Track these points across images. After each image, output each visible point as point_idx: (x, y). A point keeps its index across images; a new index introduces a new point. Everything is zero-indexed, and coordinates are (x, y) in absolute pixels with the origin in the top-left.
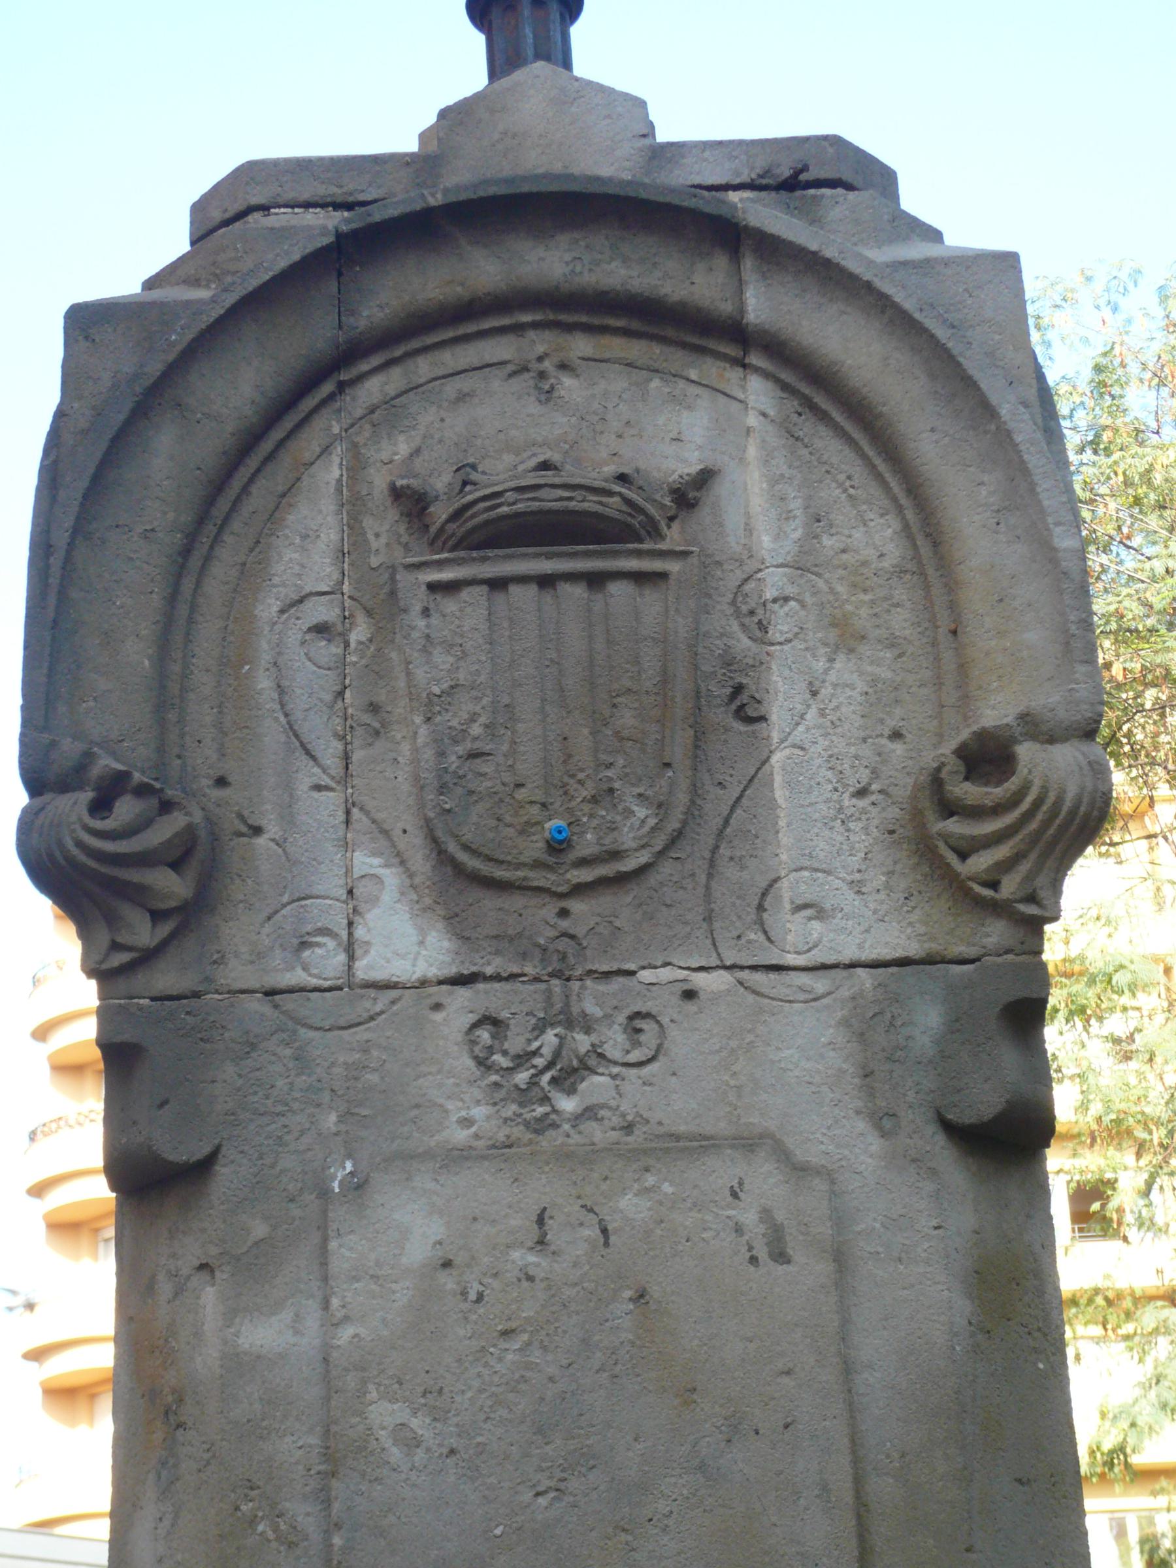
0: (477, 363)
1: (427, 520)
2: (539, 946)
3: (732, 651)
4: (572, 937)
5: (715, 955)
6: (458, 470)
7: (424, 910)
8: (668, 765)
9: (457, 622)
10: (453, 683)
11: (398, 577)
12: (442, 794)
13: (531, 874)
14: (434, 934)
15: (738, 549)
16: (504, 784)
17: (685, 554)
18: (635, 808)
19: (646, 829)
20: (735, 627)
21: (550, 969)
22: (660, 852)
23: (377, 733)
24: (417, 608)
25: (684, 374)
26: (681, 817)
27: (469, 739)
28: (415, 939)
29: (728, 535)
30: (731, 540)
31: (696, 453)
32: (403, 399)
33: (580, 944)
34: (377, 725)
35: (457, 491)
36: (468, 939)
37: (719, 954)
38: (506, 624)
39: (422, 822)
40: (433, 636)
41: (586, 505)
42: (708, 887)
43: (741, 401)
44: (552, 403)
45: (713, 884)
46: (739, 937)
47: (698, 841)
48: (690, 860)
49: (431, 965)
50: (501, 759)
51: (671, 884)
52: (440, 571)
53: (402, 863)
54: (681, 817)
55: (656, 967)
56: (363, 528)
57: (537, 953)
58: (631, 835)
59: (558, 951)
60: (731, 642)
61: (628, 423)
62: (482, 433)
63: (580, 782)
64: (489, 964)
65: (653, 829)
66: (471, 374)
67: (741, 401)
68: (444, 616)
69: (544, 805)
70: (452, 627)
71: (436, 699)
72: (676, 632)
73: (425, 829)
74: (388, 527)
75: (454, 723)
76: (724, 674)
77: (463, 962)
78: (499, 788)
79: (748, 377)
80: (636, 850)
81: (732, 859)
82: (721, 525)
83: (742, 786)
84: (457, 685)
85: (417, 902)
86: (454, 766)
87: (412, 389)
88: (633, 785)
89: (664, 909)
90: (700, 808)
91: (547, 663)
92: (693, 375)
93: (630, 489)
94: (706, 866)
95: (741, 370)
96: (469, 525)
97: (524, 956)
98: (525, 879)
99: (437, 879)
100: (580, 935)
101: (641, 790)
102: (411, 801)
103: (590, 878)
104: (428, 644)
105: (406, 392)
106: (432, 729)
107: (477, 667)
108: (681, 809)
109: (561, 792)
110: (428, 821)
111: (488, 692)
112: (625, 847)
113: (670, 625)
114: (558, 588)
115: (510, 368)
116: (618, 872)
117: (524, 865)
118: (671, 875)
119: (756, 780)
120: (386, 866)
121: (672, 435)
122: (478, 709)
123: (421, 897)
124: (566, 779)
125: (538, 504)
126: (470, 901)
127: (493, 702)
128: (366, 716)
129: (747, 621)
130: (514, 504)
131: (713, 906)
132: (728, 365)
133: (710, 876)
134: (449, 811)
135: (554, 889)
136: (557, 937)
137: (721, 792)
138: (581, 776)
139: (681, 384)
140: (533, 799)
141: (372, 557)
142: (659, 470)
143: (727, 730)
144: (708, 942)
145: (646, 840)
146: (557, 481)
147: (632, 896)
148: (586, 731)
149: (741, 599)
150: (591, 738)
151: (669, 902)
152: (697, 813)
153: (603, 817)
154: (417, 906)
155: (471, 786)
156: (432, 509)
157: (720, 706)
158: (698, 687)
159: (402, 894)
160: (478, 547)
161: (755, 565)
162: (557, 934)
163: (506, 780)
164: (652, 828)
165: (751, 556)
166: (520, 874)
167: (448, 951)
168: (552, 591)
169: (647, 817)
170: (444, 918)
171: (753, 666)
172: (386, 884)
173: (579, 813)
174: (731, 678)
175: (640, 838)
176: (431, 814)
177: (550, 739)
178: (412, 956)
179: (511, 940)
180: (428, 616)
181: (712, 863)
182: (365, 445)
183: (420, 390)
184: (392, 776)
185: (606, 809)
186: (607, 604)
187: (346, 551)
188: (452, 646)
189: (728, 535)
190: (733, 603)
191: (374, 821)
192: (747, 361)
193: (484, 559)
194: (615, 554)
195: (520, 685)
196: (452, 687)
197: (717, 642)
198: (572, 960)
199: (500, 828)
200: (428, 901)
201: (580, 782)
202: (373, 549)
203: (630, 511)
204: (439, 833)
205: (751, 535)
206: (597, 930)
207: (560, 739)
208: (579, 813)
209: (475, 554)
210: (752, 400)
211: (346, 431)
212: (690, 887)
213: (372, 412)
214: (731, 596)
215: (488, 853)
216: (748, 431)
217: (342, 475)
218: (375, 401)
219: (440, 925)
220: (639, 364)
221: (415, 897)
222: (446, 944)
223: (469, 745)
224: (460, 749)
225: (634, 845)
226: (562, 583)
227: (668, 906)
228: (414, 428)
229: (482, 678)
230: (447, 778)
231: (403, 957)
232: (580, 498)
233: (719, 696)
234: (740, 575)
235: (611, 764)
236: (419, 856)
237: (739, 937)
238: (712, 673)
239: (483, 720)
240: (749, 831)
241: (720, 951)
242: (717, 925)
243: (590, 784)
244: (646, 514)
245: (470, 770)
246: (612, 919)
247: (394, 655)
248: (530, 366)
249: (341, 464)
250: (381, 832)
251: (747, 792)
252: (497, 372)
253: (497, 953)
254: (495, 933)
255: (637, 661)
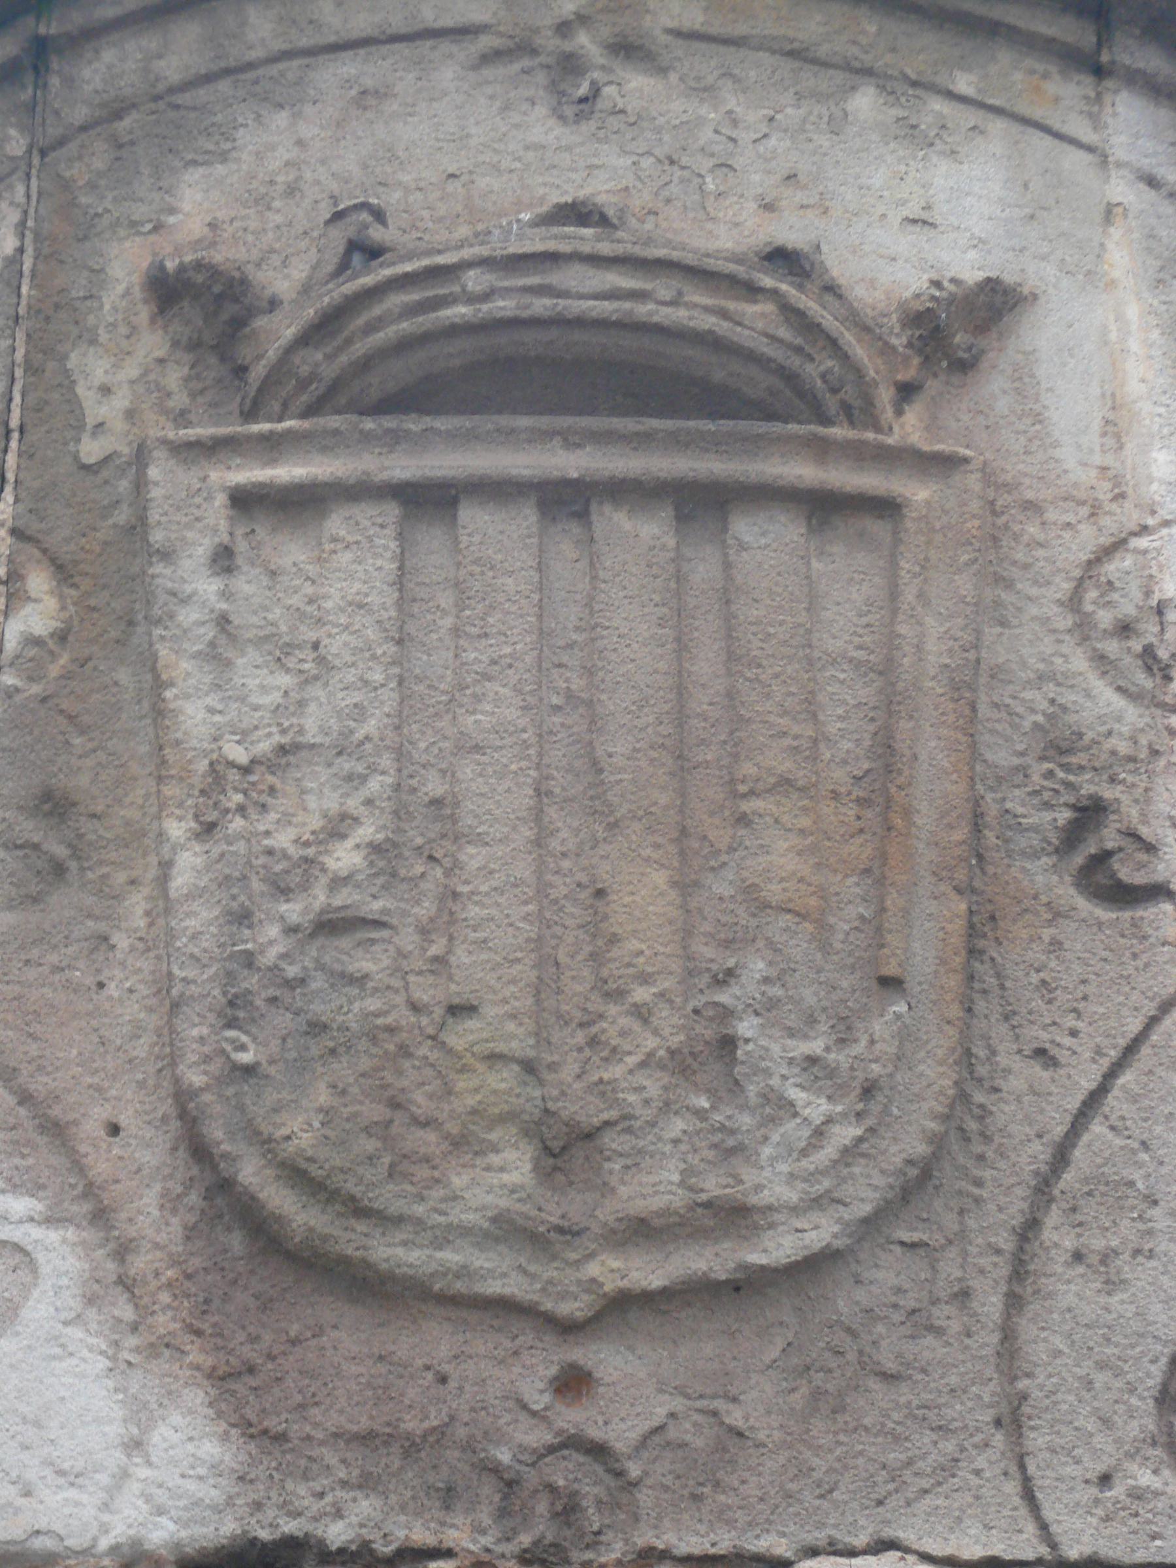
0: (398, 24)
1: (245, 353)
2: (495, 1470)
3: (1071, 718)
4: (598, 1451)
5: (1031, 1528)
6: (338, 216)
7: (152, 1350)
8: (891, 984)
9: (309, 589)
10: (285, 740)
11: (153, 473)
12: (231, 1024)
13: (481, 1260)
14: (176, 1419)
15: (1087, 477)
16: (415, 1007)
17: (946, 464)
18: (797, 1095)
19: (828, 1152)
20: (1079, 662)
21: (525, 1540)
22: (866, 1221)
23: (59, 869)
24: (202, 549)
25: (941, 80)
26: (932, 1125)
27: (324, 880)
28: (114, 1430)
29: (1056, 445)
30: (1068, 456)
31: (972, 254)
32: (202, 94)
33: (619, 1474)
34: (61, 851)
35: (330, 268)
36: (281, 1438)
37: (1044, 1527)
38: (446, 599)
39: (166, 1107)
40: (236, 621)
41: (678, 316)
42: (1008, 1334)
43: (1090, 149)
44: (593, 124)
45: (1026, 1328)
46: (1105, 1480)
47: (978, 1200)
48: (953, 1253)
49: (160, 1511)
50: (408, 939)
51: (897, 1317)
52: (273, 462)
53: (101, 1216)
54: (932, 1125)
55: (852, 1553)
56: (67, 373)
57: (489, 1490)
58: (784, 1168)
59: (551, 1488)
60: (1068, 697)
61: (791, 177)
62: (406, 178)
63: (642, 1013)
64: (339, 1513)
65: (849, 1153)
66: (385, 49)
67: (1090, 149)
68: (273, 574)
69: (529, 1067)
70: (295, 601)
71: (233, 776)
72: (919, 648)
73: (175, 1124)
74: (134, 373)
75: (283, 840)
76: (1050, 774)
77: (258, 1506)
78: (402, 1016)
79: (1108, 99)
80: (795, 1210)
81: (1078, 1256)
82: (1038, 418)
83: (1105, 1063)
84: (297, 747)
85: (134, 1328)
86: (272, 953)
87: (227, 72)
88: (791, 1033)
89: (873, 1384)
90: (984, 1113)
91: (555, 700)
92: (964, 84)
93: (800, 287)
94: (1005, 1271)
95: (1088, 80)
96: (360, 348)
97: (448, 1496)
98: (463, 1272)
99: (196, 1263)
100: (619, 1446)
101: (816, 1047)
102: (141, 1048)
103: (656, 1281)
104: (223, 640)
105: (208, 78)
106: (216, 851)
107: (356, 697)
108: (932, 1104)
109: (580, 1037)
110: (182, 1096)
111: (386, 761)
112: (765, 1197)
113: (903, 629)
114: (599, 525)
115: (486, 42)
116: (744, 1267)
117: (465, 1231)
118: (899, 1290)
119: (1145, 1050)
120: (49, 1221)
121: (906, 212)
122: (353, 804)
123: (144, 1312)
124: (596, 1004)
125: (548, 302)
126: (294, 1329)
127: (397, 787)
128: (29, 825)
129: (1112, 647)
130: (486, 296)
131: (1022, 1384)
132: (1053, 69)
133: (1014, 1302)
134: (249, 1070)
135: (548, 1305)
136: (551, 1449)
137: (1046, 1075)
138: (641, 994)
139: (938, 105)
140: (501, 1047)
141: (86, 438)
142: (872, 284)
143: (1057, 915)
144: (1012, 1488)
145: (826, 1183)
146: (605, 248)
147: (780, 1343)
148: (660, 878)
149: (1092, 594)
150: (673, 894)
151: (891, 1366)
152: (972, 1125)
153: (700, 1114)
154: (132, 1341)
155: (319, 1009)
156: (260, 322)
157: (1035, 855)
158: (977, 802)
159: (91, 1300)
160: (380, 408)
161: (1131, 516)
162: (549, 1438)
163: (423, 996)
164: (846, 1151)
165: (1122, 496)
166: (451, 1257)
167: (216, 1469)
168: (575, 528)
169: (829, 1121)
170: (212, 1375)
171: (1132, 759)
172: (45, 1270)
173: (632, 1098)
174: (1069, 785)
175: (810, 1177)
176: (196, 1079)
177: (553, 894)
178: (104, 1478)
179: (411, 1447)
180: (229, 570)
181: (1019, 1271)
182: (92, 186)
183: (250, 75)
184: (90, 981)
185: (711, 1093)
186: (727, 566)
187: (14, 422)
188: (289, 648)
189: (1056, 445)
190: (1073, 602)
191: (25, 1098)
192: (1105, 58)
193: (394, 439)
194: (755, 445)
195: (477, 748)
196: (282, 750)
197: (1028, 695)
198: (594, 1519)
199: (395, 1129)
200: (164, 1322)
201: (642, 1013)
202: (90, 421)
203: (799, 341)
204: (215, 1132)
205: (1121, 447)
206: (672, 1433)
207: (584, 895)
208: (632, 1098)
209: (369, 424)
210: (1120, 145)
211: (43, 153)
212: (955, 1326)
213: (118, 115)
214: (1067, 586)
215: (357, 1191)
216: (1109, 213)
217: (21, 250)
218: (128, 91)
219: (196, 1397)
220: (823, 51)
221: (128, 1313)
222: (210, 1449)
223: (319, 897)
224: (293, 910)
225: (791, 1195)
226: (607, 509)
227: (889, 1377)
228: (224, 157)
229: (371, 726)
230: (250, 982)
231: (72, 1477)
232: (665, 294)
233: (1035, 829)
234: (1087, 540)
235: (730, 973)
236: (150, 1200)
237: (1105, 1480)
238: (1017, 769)
239: (366, 832)
240: (1131, 1184)
241: (1048, 1514)
242: (1036, 1440)
243: (666, 1019)
244: (844, 357)
245: (320, 966)
246: (719, 1404)
247: (123, 675)
248: (538, 41)
249: (22, 224)
250: (42, 1129)
251: (1121, 1081)
252: (454, 48)
253: (367, 1483)
254: (363, 1424)
255: (811, 710)
